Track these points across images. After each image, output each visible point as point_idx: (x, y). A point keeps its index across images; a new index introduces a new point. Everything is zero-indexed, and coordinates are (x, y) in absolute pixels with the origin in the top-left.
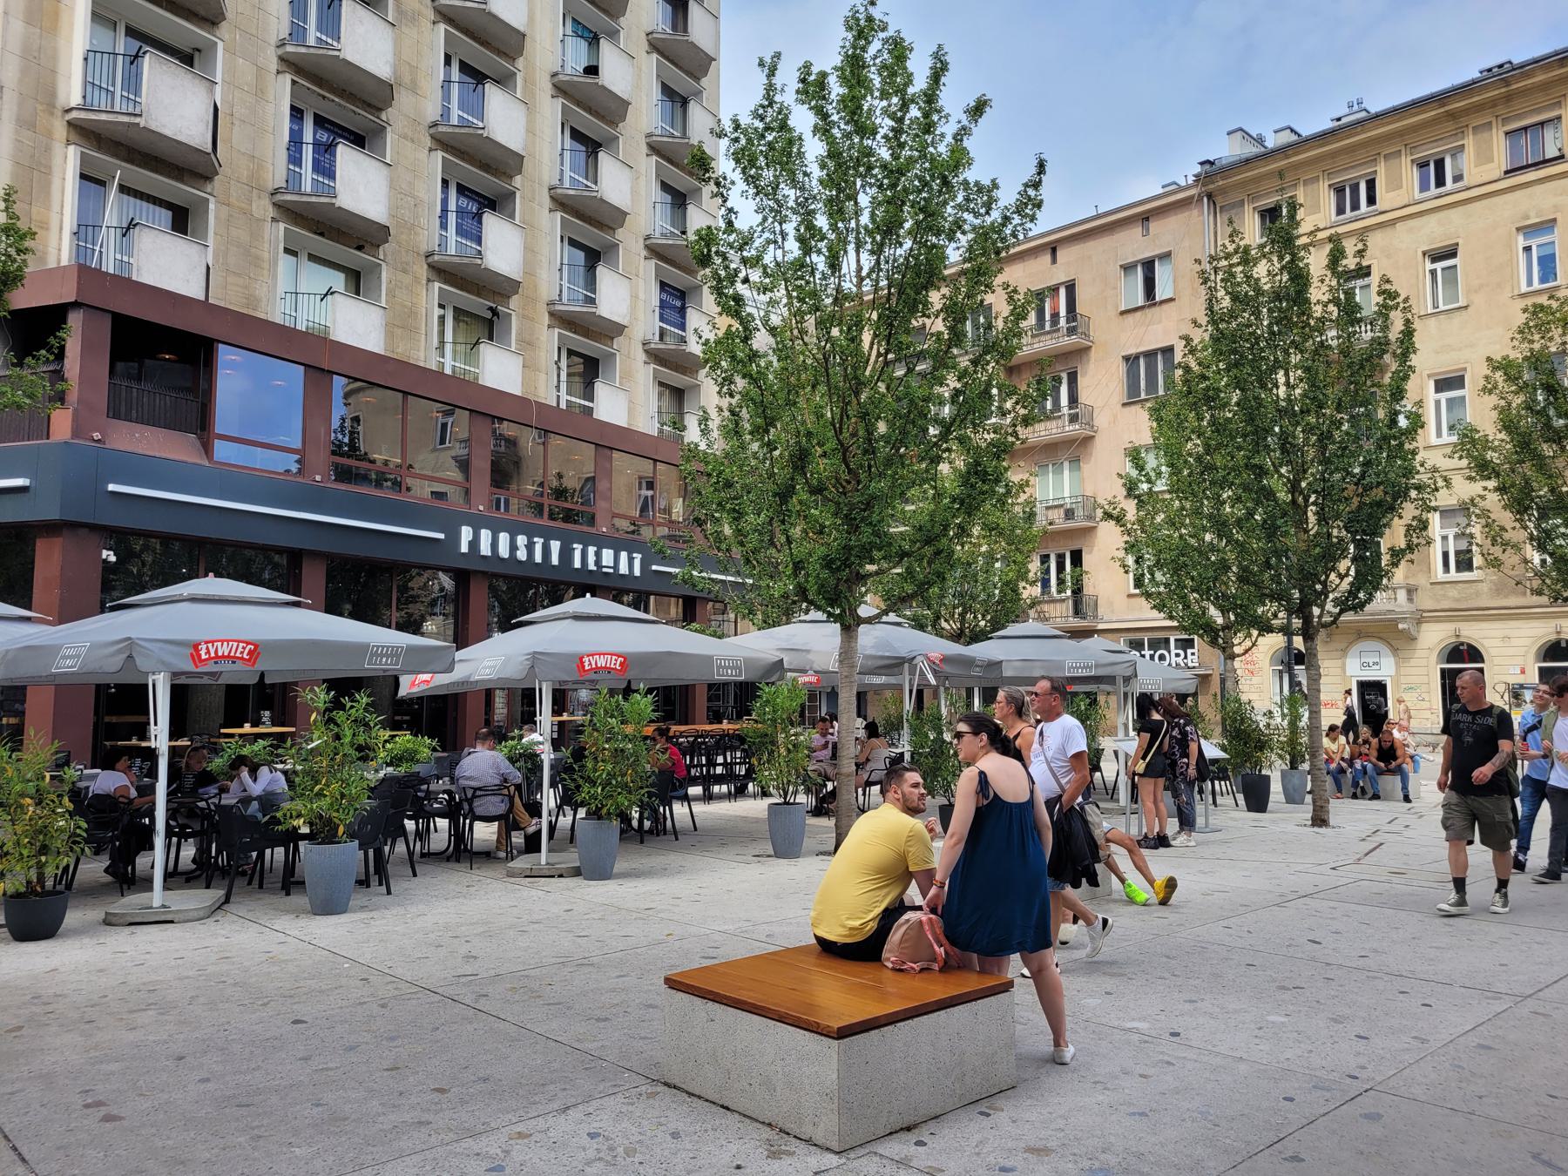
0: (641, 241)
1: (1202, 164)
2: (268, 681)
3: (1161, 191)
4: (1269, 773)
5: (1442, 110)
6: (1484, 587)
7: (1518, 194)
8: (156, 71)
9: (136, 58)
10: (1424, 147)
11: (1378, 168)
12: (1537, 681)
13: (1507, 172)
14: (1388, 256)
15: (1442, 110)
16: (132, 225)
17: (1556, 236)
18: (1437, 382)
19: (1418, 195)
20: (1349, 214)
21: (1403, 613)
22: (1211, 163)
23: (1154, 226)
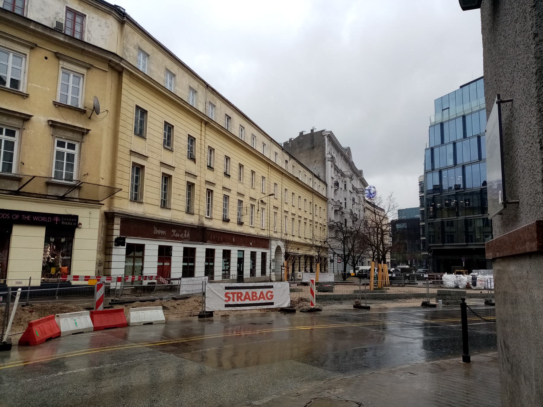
2: (315, 131)
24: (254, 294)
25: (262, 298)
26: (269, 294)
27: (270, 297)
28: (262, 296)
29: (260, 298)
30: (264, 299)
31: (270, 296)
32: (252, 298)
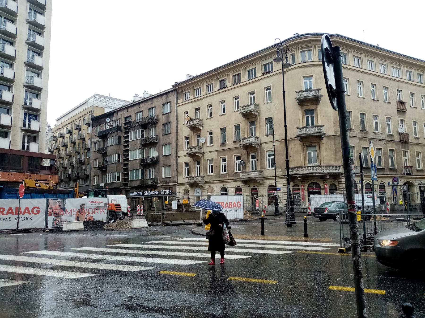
0: (20, 129)
1: (176, 83)
3: (293, 36)
4: (313, 209)
5: (208, 76)
6: (214, 176)
7: (220, 94)
8: (38, 15)
9: (3, 44)
10: (207, 83)
11: (256, 67)
12: (242, 196)
13: (219, 89)
14: (202, 106)
15: (208, 76)
16: (33, 56)
17: (255, 95)
18: (271, 118)
19: (207, 93)
20: (198, 96)
21: (200, 182)
22: (177, 83)
23: (130, 110)
24: (231, 204)
25: (235, 206)
26: (238, 204)
27: (239, 206)
28: (235, 205)
29: (25, 212)
30: (236, 207)
31: (239, 205)
32: (230, 206)
